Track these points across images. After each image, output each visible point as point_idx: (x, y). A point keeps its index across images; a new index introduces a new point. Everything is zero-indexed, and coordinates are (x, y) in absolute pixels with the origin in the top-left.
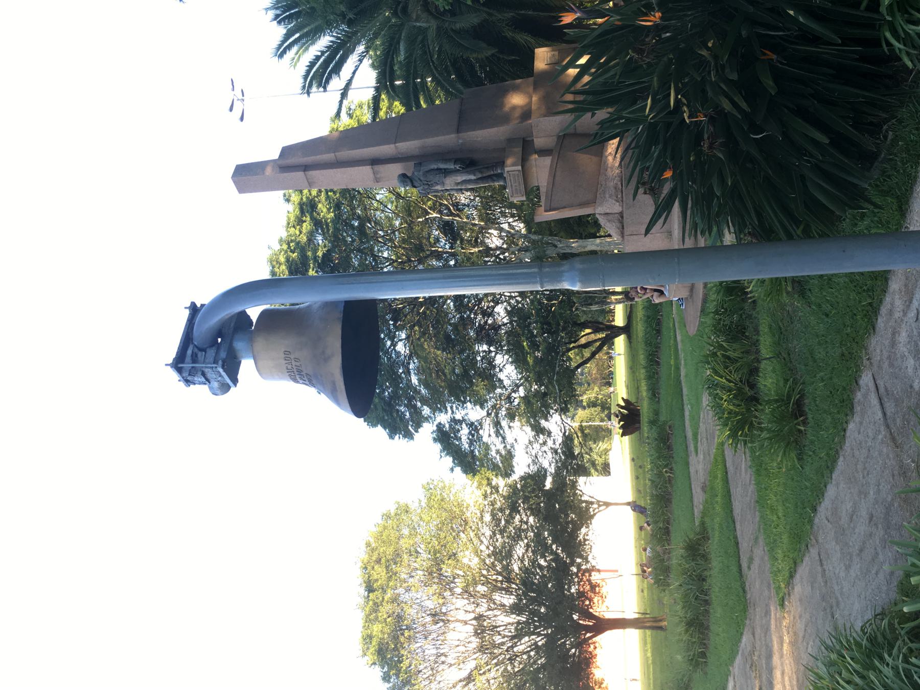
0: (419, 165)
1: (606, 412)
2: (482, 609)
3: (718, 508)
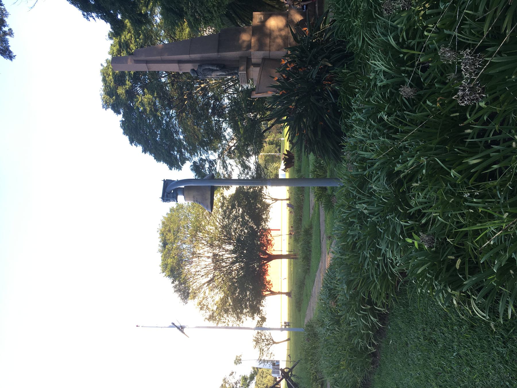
0: (200, 66)
1: (278, 148)
2: (217, 251)
3: (316, 219)
